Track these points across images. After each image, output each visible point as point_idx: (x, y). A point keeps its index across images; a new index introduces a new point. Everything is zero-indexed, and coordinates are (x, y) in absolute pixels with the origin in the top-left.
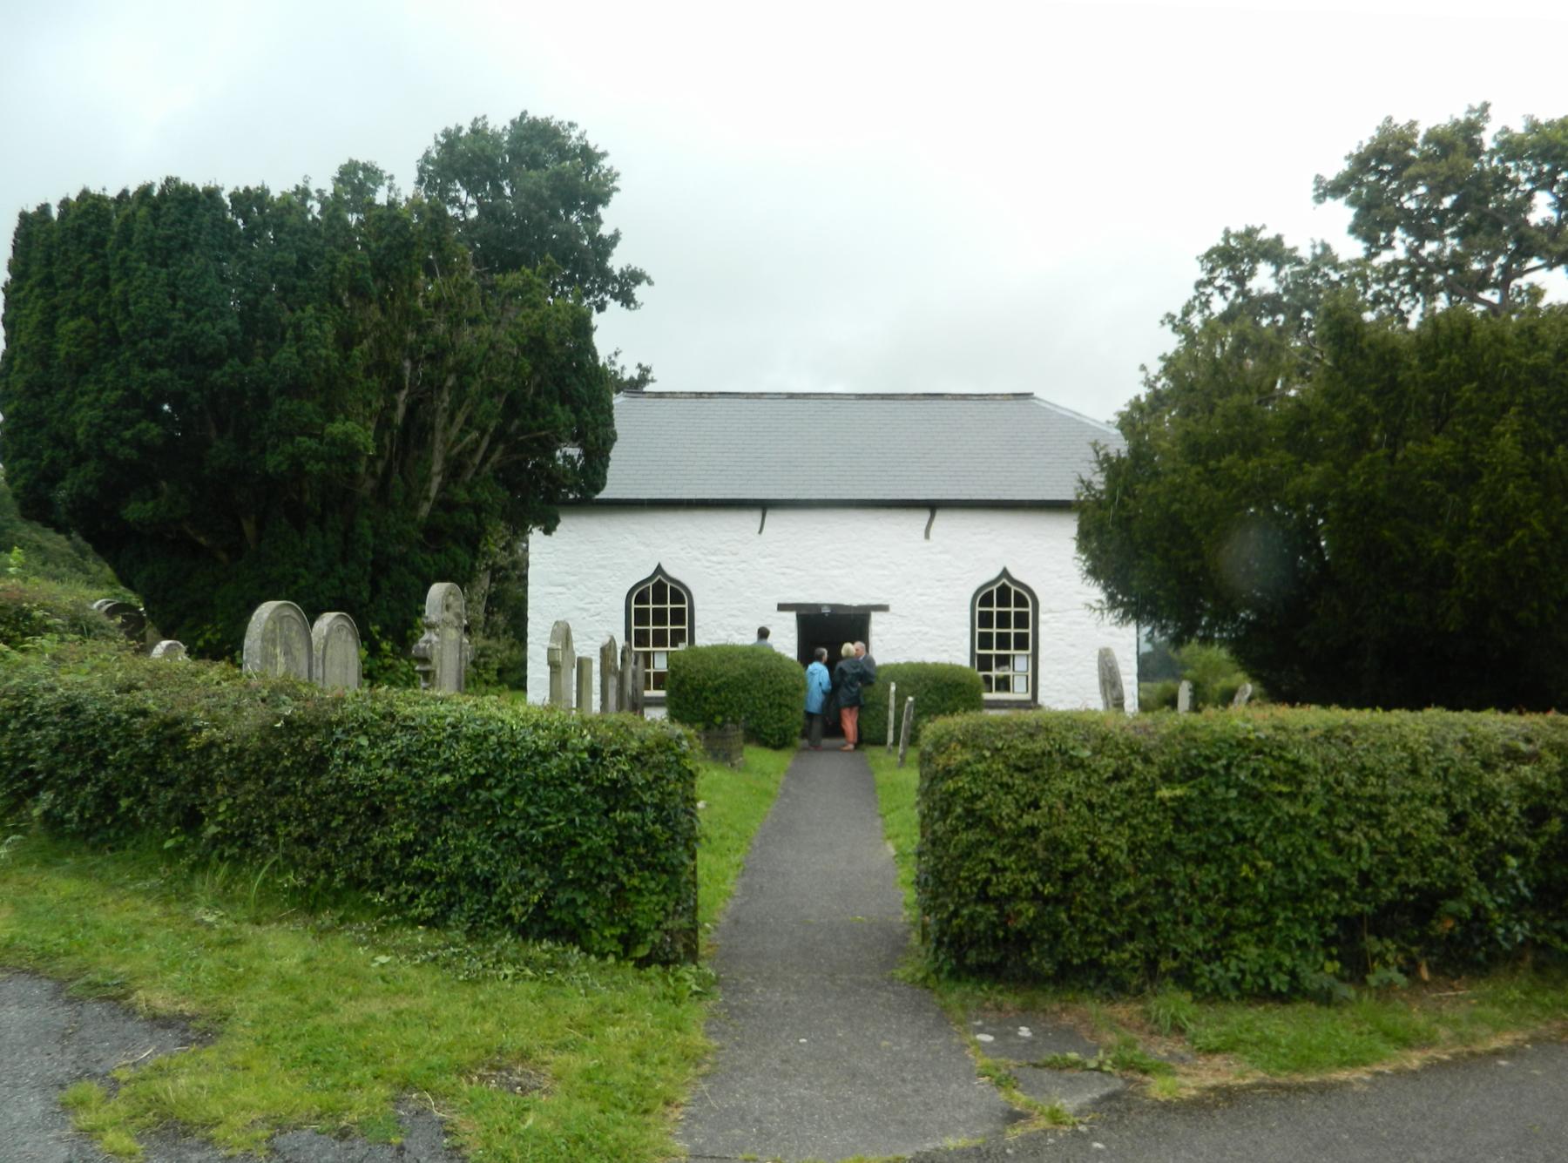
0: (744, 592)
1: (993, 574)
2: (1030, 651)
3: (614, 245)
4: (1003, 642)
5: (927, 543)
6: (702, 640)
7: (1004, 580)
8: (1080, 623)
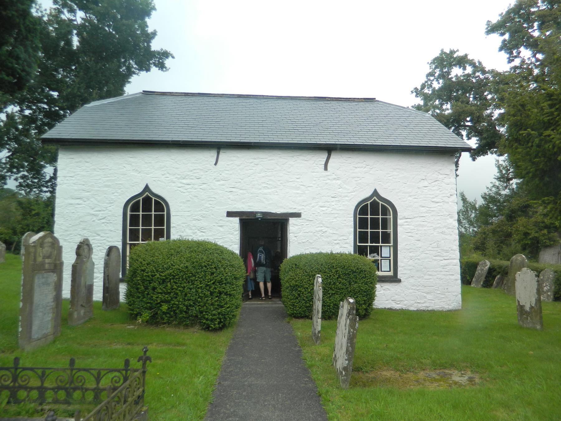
0: (207, 204)
1: (368, 193)
2: (392, 244)
3: (153, 38)
4: (375, 237)
5: (326, 173)
6: (174, 236)
7: (375, 198)
8: (423, 226)
